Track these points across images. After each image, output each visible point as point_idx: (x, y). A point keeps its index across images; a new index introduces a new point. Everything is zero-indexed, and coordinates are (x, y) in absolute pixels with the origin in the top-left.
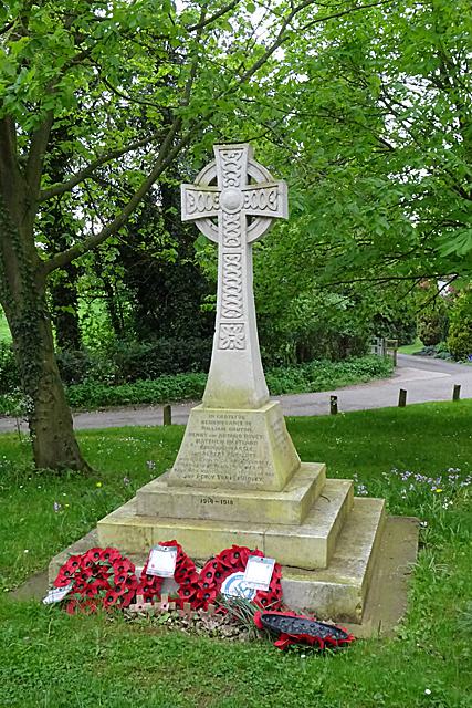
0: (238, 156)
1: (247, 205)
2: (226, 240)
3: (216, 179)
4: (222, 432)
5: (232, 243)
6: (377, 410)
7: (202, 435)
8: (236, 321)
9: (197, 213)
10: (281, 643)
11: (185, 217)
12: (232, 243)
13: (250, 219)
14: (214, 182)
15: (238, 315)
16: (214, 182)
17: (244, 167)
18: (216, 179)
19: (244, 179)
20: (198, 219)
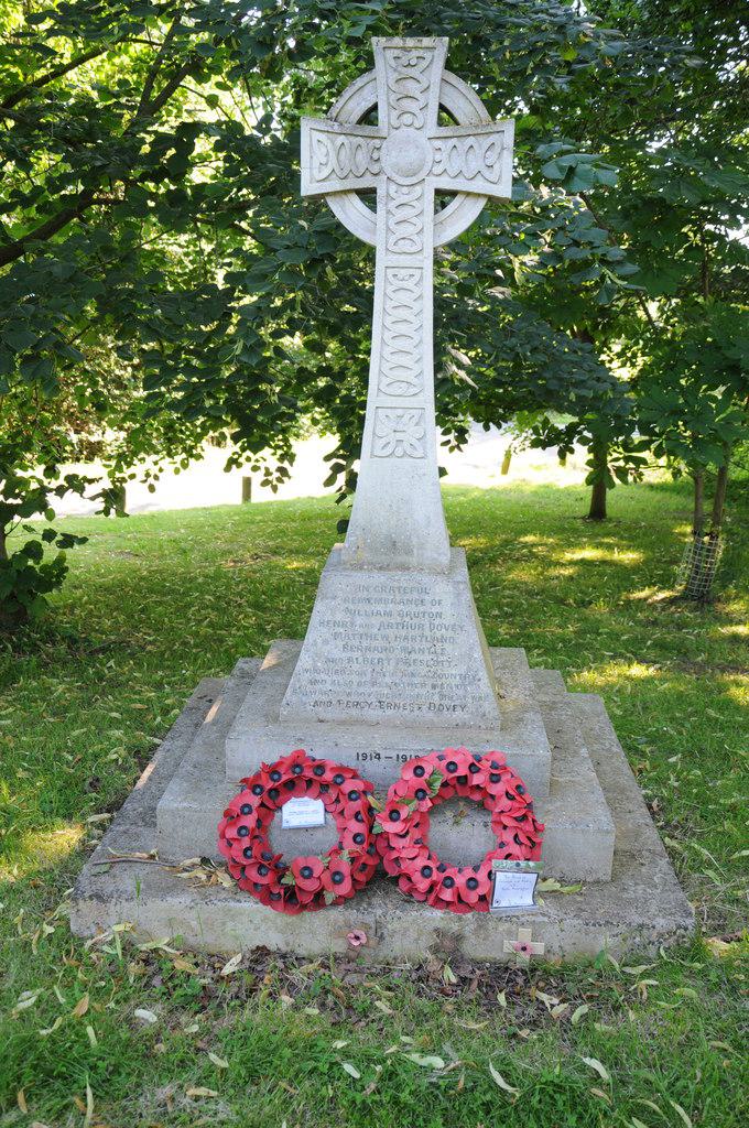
0: (424, 64)
1: (438, 169)
2: (392, 239)
3: (375, 108)
4: (386, 619)
5: (405, 246)
6: (196, 566)
7: (344, 625)
8: (407, 402)
9: (461, 179)
10: (196, 1007)
11: (308, 188)
12: (405, 246)
13: (443, 197)
14: (369, 117)
15: (413, 390)
16: (369, 117)
17: (435, 89)
18: (375, 108)
19: (433, 113)
20: (335, 193)
